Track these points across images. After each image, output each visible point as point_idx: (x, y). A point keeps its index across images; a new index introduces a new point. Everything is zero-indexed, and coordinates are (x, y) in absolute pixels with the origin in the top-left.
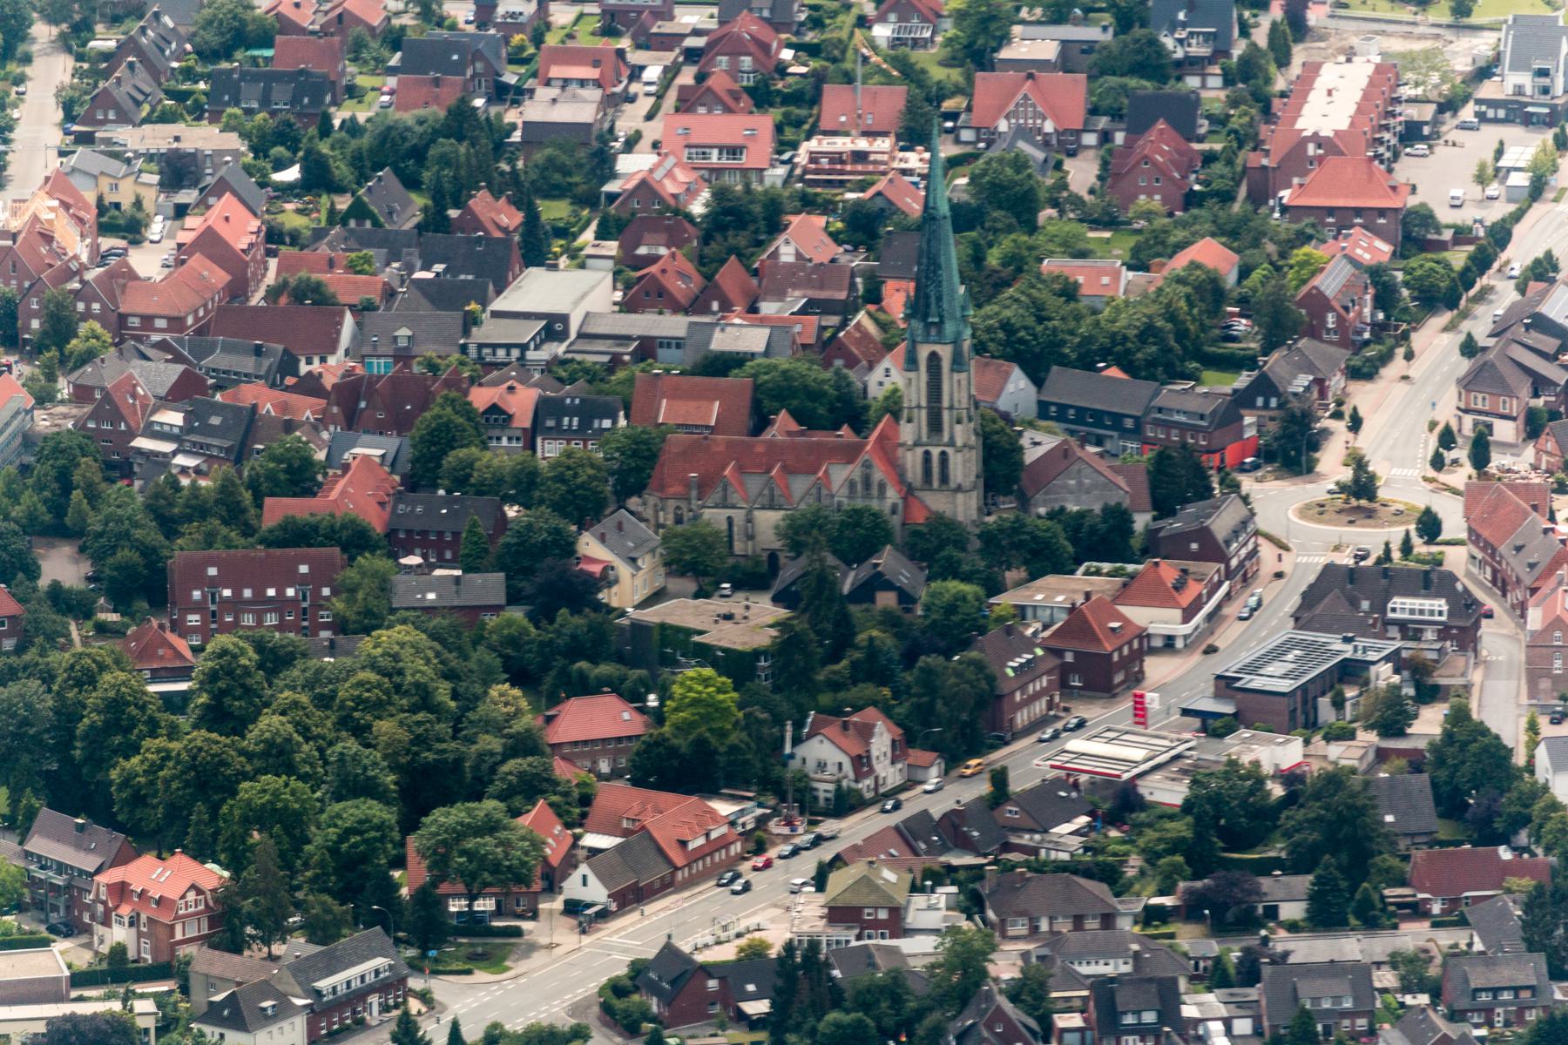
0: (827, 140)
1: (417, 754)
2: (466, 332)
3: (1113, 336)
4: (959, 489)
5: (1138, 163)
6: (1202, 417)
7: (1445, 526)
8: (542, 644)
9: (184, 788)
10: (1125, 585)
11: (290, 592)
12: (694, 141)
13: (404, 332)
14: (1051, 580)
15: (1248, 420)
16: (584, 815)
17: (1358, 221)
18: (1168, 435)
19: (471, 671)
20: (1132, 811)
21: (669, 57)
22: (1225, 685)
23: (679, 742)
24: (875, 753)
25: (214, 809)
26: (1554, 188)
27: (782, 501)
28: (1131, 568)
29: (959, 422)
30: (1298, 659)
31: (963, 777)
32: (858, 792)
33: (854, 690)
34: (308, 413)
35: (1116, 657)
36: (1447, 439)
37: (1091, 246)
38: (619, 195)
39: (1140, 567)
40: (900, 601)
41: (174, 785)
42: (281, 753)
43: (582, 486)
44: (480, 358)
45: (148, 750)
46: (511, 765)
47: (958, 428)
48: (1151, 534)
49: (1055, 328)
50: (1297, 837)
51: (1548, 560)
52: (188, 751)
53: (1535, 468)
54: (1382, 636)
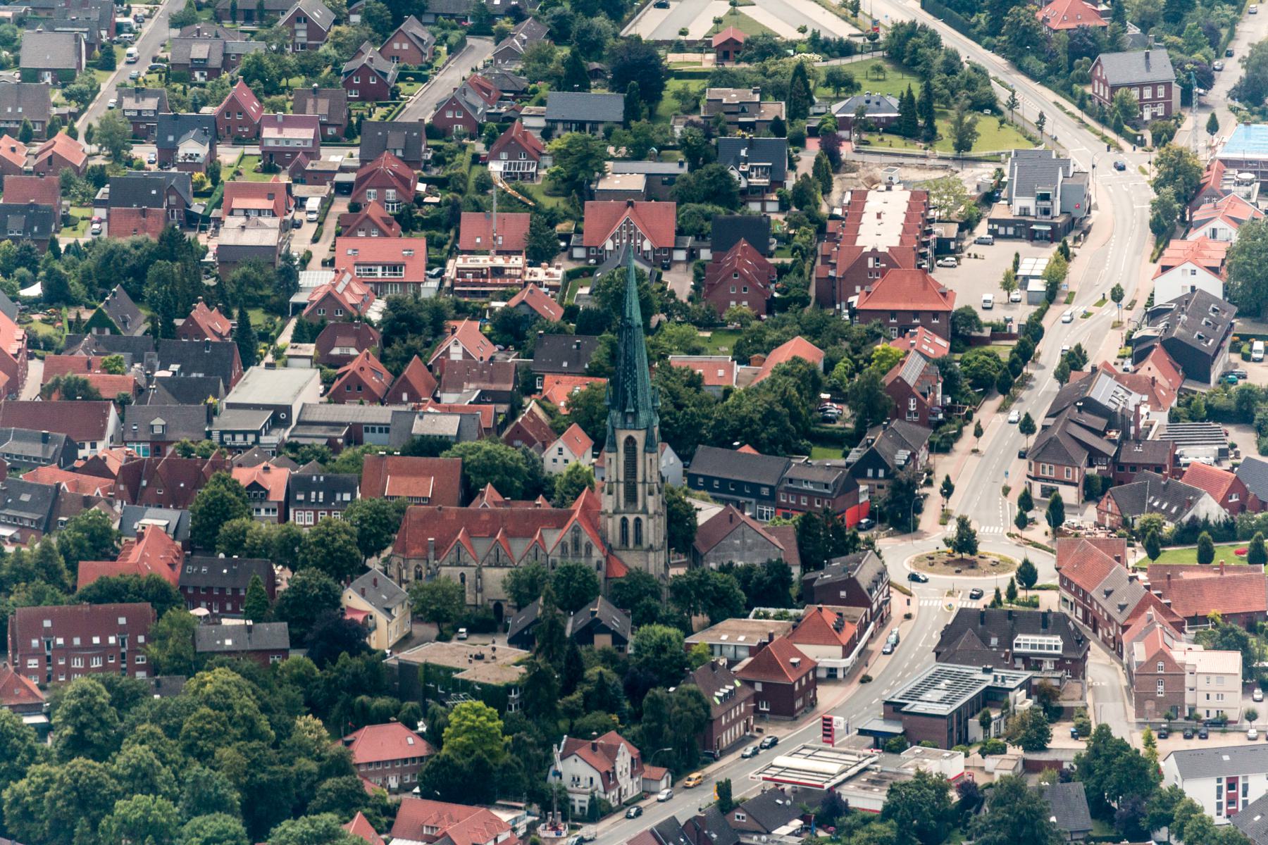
0: (470, 258)
1: (253, 775)
2: (210, 422)
3: (742, 419)
4: (651, 548)
5: (729, 276)
6: (827, 486)
7: (1039, 574)
8: (329, 682)
9: (67, 806)
10: (794, 627)
11: (112, 640)
12: (361, 260)
13: (158, 422)
14: (731, 623)
15: (863, 488)
16: (390, 825)
17: (916, 321)
18: (798, 501)
19: (280, 705)
20: (839, 815)
21: (327, 189)
22: (894, 709)
23: (461, 762)
24: (618, 769)
25: (94, 825)
26: (1064, 293)
27: (506, 559)
28: (792, 612)
29: (651, 493)
30: (949, 688)
31: (687, 787)
32: (606, 801)
33: (589, 717)
34: (98, 490)
35: (797, 687)
36: (1026, 502)
37: (701, 345)
38: (304, 306)
39: (801, 612)
40: (614, 643)
41: (59, 804)
42: (145, 775)
43: (339, 549)
44: (222, 442)
45: (34, 774)
46: (329, 783)
47: (650, 499)
48: (807, 585)
49: (692, 414)
50: (985, 837)
51: (1137, 602)
52: (71, 775)
53: (1098, 525)
54: (1012, 667)
